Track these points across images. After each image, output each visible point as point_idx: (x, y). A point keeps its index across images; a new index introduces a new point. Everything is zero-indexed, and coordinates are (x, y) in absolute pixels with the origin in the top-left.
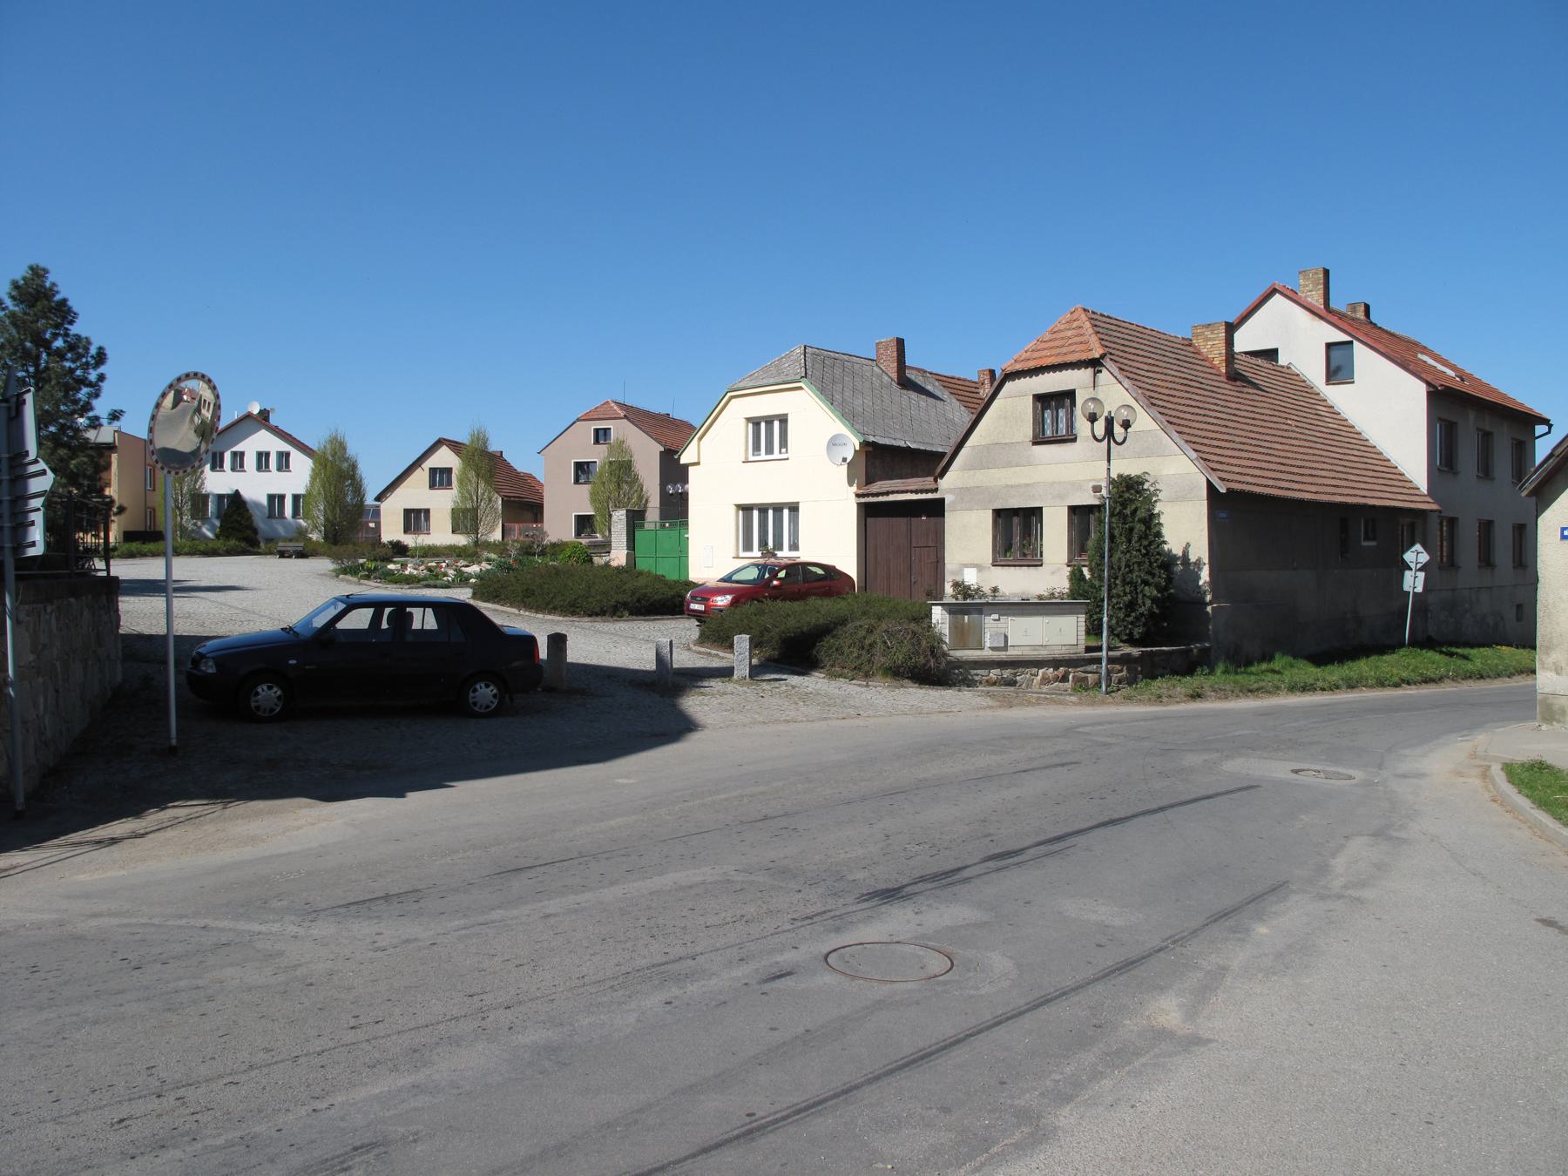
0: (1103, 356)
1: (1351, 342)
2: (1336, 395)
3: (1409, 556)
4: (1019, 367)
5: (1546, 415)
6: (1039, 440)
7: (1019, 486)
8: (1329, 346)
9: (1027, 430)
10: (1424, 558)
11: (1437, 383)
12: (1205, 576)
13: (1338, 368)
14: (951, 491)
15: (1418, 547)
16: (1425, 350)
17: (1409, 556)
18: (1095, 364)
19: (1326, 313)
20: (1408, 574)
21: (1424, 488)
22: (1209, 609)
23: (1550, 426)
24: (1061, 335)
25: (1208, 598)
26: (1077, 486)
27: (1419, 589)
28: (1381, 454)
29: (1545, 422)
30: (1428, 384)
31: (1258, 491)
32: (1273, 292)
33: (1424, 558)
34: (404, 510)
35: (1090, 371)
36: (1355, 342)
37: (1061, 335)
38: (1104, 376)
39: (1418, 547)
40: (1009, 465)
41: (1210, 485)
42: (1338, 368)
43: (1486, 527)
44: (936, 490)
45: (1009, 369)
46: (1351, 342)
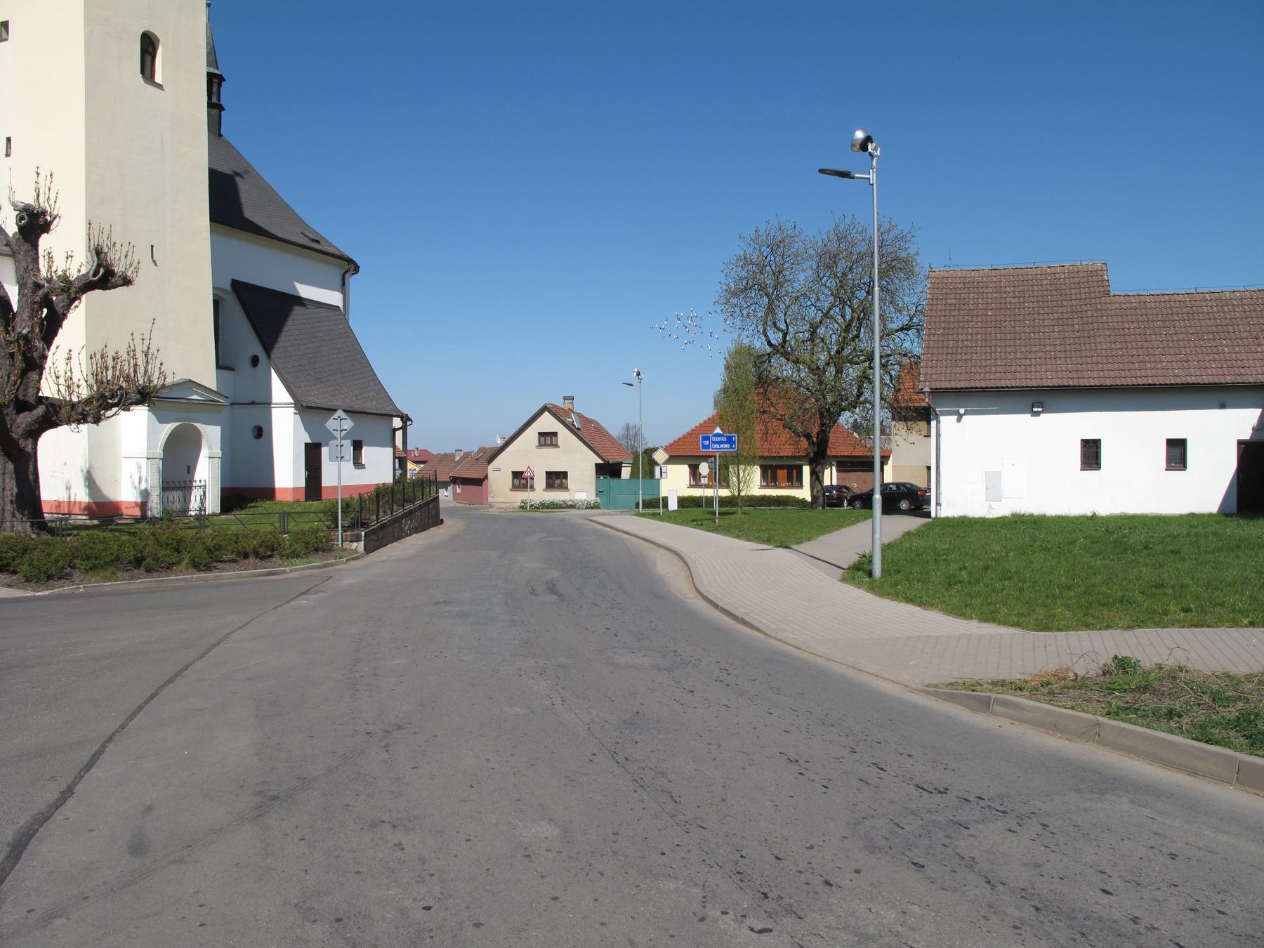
29: (410, 420)
34: (1100, 440)
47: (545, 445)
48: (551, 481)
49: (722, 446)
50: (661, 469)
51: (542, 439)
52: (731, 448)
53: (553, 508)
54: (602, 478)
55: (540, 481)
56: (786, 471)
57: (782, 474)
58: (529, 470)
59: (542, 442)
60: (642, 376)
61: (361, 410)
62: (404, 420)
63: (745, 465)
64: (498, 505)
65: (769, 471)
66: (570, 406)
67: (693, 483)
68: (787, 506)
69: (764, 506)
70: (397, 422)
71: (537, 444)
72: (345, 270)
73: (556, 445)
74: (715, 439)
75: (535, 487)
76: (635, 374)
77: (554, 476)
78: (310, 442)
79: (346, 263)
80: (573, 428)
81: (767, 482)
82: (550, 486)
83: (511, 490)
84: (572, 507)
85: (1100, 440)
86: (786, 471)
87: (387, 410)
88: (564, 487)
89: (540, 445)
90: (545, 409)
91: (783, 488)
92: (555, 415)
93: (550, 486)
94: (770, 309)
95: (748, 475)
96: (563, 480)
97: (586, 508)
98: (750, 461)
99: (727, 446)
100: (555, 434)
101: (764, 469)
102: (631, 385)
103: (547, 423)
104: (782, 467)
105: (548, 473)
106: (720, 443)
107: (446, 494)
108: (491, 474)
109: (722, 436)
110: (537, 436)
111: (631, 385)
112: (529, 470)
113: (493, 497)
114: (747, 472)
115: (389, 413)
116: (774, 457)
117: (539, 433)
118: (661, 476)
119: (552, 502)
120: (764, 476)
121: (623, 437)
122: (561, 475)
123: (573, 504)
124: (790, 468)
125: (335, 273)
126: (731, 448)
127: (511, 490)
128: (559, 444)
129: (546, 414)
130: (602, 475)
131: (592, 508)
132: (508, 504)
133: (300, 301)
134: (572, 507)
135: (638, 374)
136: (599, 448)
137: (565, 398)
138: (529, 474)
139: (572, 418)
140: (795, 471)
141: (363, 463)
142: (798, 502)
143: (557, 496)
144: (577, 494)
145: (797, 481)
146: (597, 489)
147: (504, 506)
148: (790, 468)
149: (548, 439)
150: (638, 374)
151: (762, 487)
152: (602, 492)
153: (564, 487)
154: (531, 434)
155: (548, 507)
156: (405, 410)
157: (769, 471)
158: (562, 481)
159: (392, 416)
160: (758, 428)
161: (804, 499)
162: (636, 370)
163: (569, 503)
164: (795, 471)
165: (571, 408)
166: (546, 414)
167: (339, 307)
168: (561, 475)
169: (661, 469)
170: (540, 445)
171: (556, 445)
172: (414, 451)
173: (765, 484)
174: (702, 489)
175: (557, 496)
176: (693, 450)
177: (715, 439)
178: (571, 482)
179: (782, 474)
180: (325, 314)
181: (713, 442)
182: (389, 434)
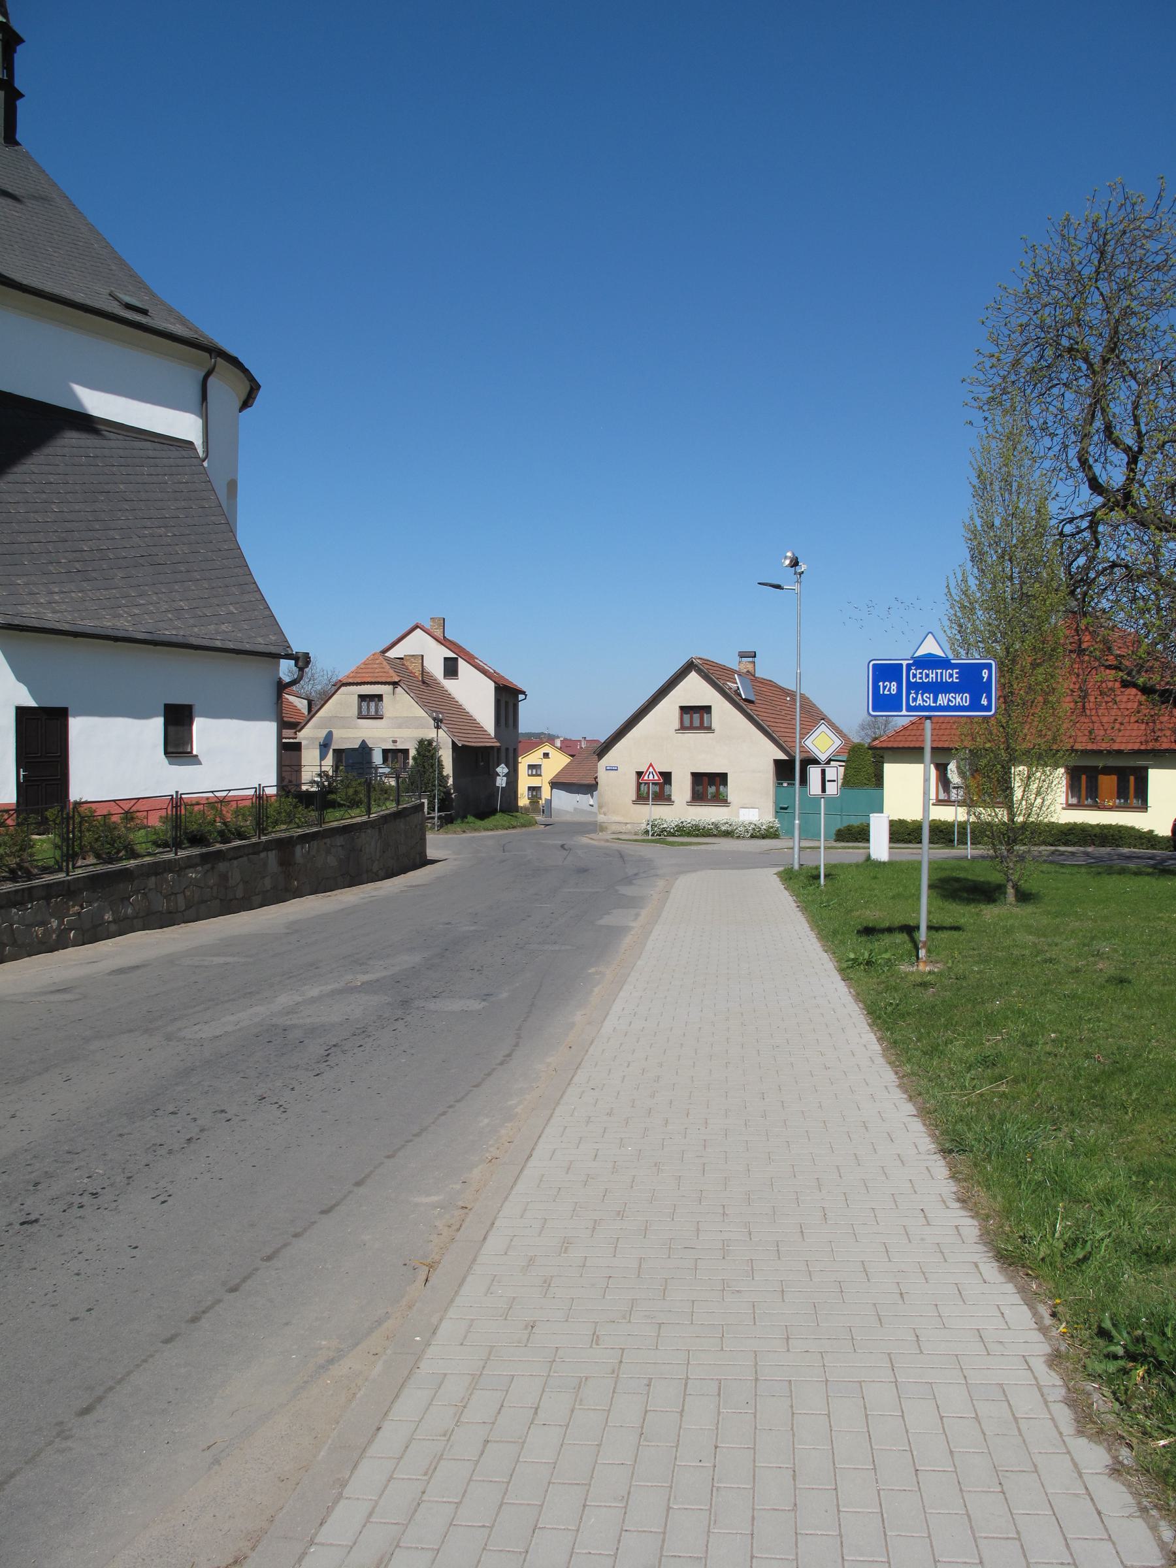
0: (400, 681)
1: (456, 659)
2: (449, 685)
3: (499, 770)
4: (351, 680)
5: (524, 689)
6: (361, 717)
7: (350, 738)
8: (445, 659)
9: (354, 711)
10: (506, 770)
11: (500, 683)
12: (450, 781)
13: (451, 669)
14: (305, 738)
15: (503, 765)
16: (477, 659)
17: (499, 770)
18: (395, 684)
19: (444, 642)
20: (498, 778)
21: (492, 733)
22: (453, 796)
23: (526, 695)
24: (370, 666)
25: (452, 791)
26: (384, 740)
27: (504, 785)
28: (475, 720)
29: (523, 693)
30: (495, 682)
31: (1094, 822)
32: (416, 627)
33: (506, 770)
34: (726, 774)
35: (391, 687)
36: (459, 659)
37: (370, 666)
38: (399, 690)
39: (503, 765)
40: (344, 727)
41: (453, 743)
42: (451, 669)
43: (507, 749)
44: (296, 738)
45: (344, 681)
46: (456, 659)
47: (691, 728)
48: (700, 788)
49: (942, 700)
50: (823, 772)
51: (687, 717)
52: (975, 705)
53: (697, 836)
54: (785, 785)
55: (681, 788)
56: (1114, 778)
57: (1108, 783)
58: (651, 770)
59: (687, 723)
60: (803, 567)
61: (181, 640)
62: (300, 664)
63: (1030, 766)
64: (614, 828)
65: (1084, 777)
66: (750, 667)
67: (942, 796)
68: (1118, 846)
69: (1074, 845)
70: (286, 669)
71: (677, 726)
72: (206, 370)
73: (709, 729)
74: (919, 676)
75: (673, 798)
76: (787, 562)
77: (706, 779)
78: (32, 703)
79: (207, 355)
80: (737, 699)
81: (1079, 798)
82: (698, 797)
83: (634, 802)
84: (728, 834)
85: (726, 774)
86: (1114, 778)
87: (260, 643)
88: (721, 800)
89: (683, 728)
90: (689, 667)
91: (1110, 809)
92: (707, 677)
93: (698, 797)
94: (1098, 401)
95: (1038, 794)
96: (722, 787)
97: (752, 837)
98: (1043, 757)
99: (962, 699)
100: (707, 709)
101: (1074, 775)
102: (778, 587)
103: (694, 690)
104: (1107, 771)
105: (694, 775)
106: (937, 688)
107: (591, 803)
108: (603, 776)
109: (943, 663)
110: (677, 712)
111: (778, 587)
112: (651, 770)
113: (605, 814)
114: (1034, 787)
115: (273, 649)
116: (1098, 753)
117: (682, 708)
118: (824, 790)
119: (696, 826)
120: (1073, 786)
121: (869, 725)
122: (718, 779)
123: (730, 829)
124: (1122, 774)
125: (187, 378)
126: (975, 705)
127: (634, 802)
128: (713, 726)
129: (693, 676)
130: (785, 780)
131: (764, 837)
132: (629, 826)
133: (86, 423)
134: (728, 834)
135: (795, 563)
136: (779, 734)
137: (743, 655)
138: (651, 777)
139: (737, 683)
140: (1132, 778)
141: (195, 752)
142: (1140, 838)
143: (708, 814)
144: (742, 811)
145: (1136, 797)
146: (776, 803)
147: (623, 828)
148: (1122, 774)
149: (696, 716)
150: (795, 563)
151: (1069, 806)
152: (786, 809)
153: (721, 800)
154: (669, 708)
155: (689, 834)
156: (297, 647)
157: (1084, 777)
158: (718, 790)
159: (278, 656)
160: (1065, 684)
161: (1151, 832)
162: (789, 554)
163: (723, 828)
164: (1132, 778)
165: (751, 669)
166: (693, 676)
167: (191, 443)
168: (718, 779)
169: (823, 772)
170: (683, 728)
171: (709, 729)
172: (580, 741)
173: (1074, 801)
174: (954, 807)
175: (708, 814)
176: (944, 738)
177: (919, 676)
178: (733, 790)
179: (1108, 783)
180: (151, 453)
181: (911, 687)
182: (270, 693)
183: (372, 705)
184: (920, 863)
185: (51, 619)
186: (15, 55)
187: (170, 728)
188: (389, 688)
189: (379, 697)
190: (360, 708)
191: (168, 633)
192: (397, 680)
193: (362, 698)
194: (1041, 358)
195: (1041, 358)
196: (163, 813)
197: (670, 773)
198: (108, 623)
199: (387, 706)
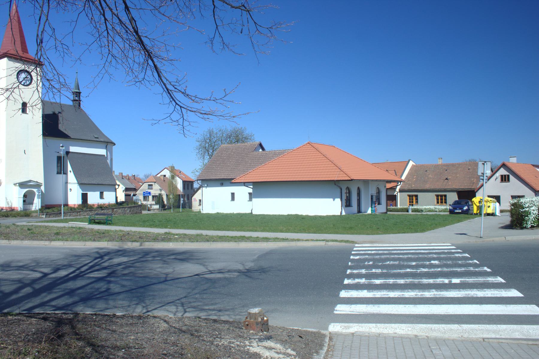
18: (155, 182)
38: (156, 183)
87: (113, 184)
103: (503, 172)
183: (151, 187)
184: (484, 216)
185: (86, 182)
186: (235, 213)
187: (388, 201)
188: (154, 183)
189: (152, 185)
190: (148, 187)
191: (100, 183)
192: (155, 181)
193: (149, 185)
194: (129, 348)
195: (129, 348)
196: (201, 211)
197: (234, 193)
198: (93, 182)
199: (154, 187)
